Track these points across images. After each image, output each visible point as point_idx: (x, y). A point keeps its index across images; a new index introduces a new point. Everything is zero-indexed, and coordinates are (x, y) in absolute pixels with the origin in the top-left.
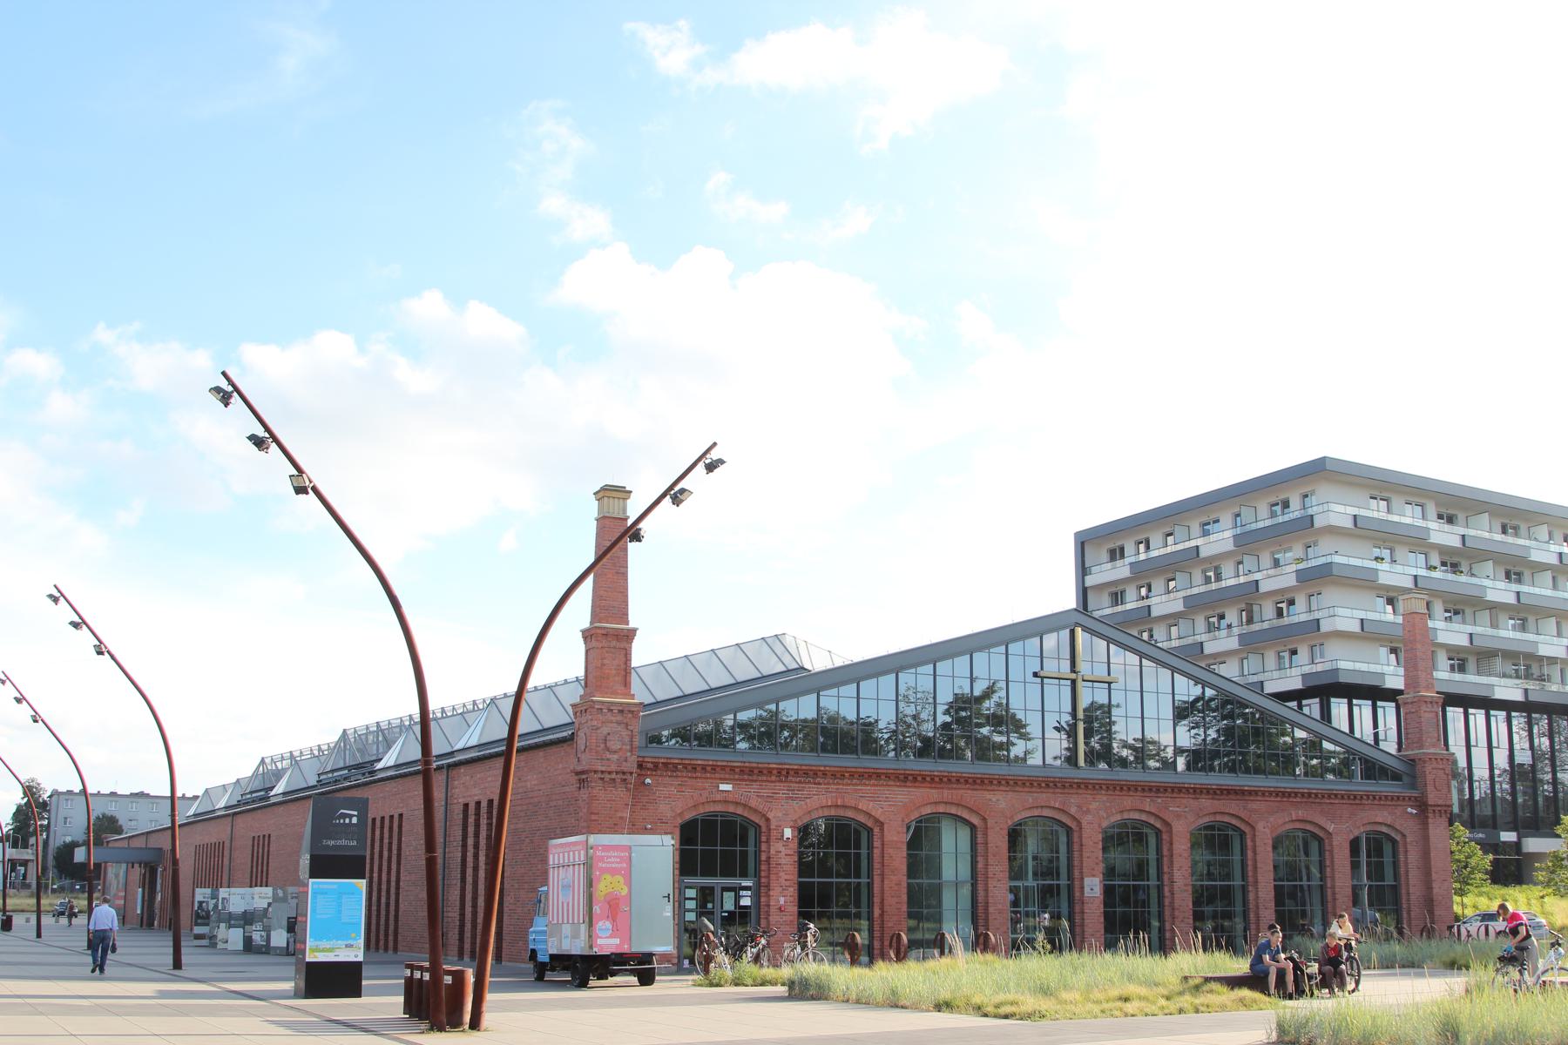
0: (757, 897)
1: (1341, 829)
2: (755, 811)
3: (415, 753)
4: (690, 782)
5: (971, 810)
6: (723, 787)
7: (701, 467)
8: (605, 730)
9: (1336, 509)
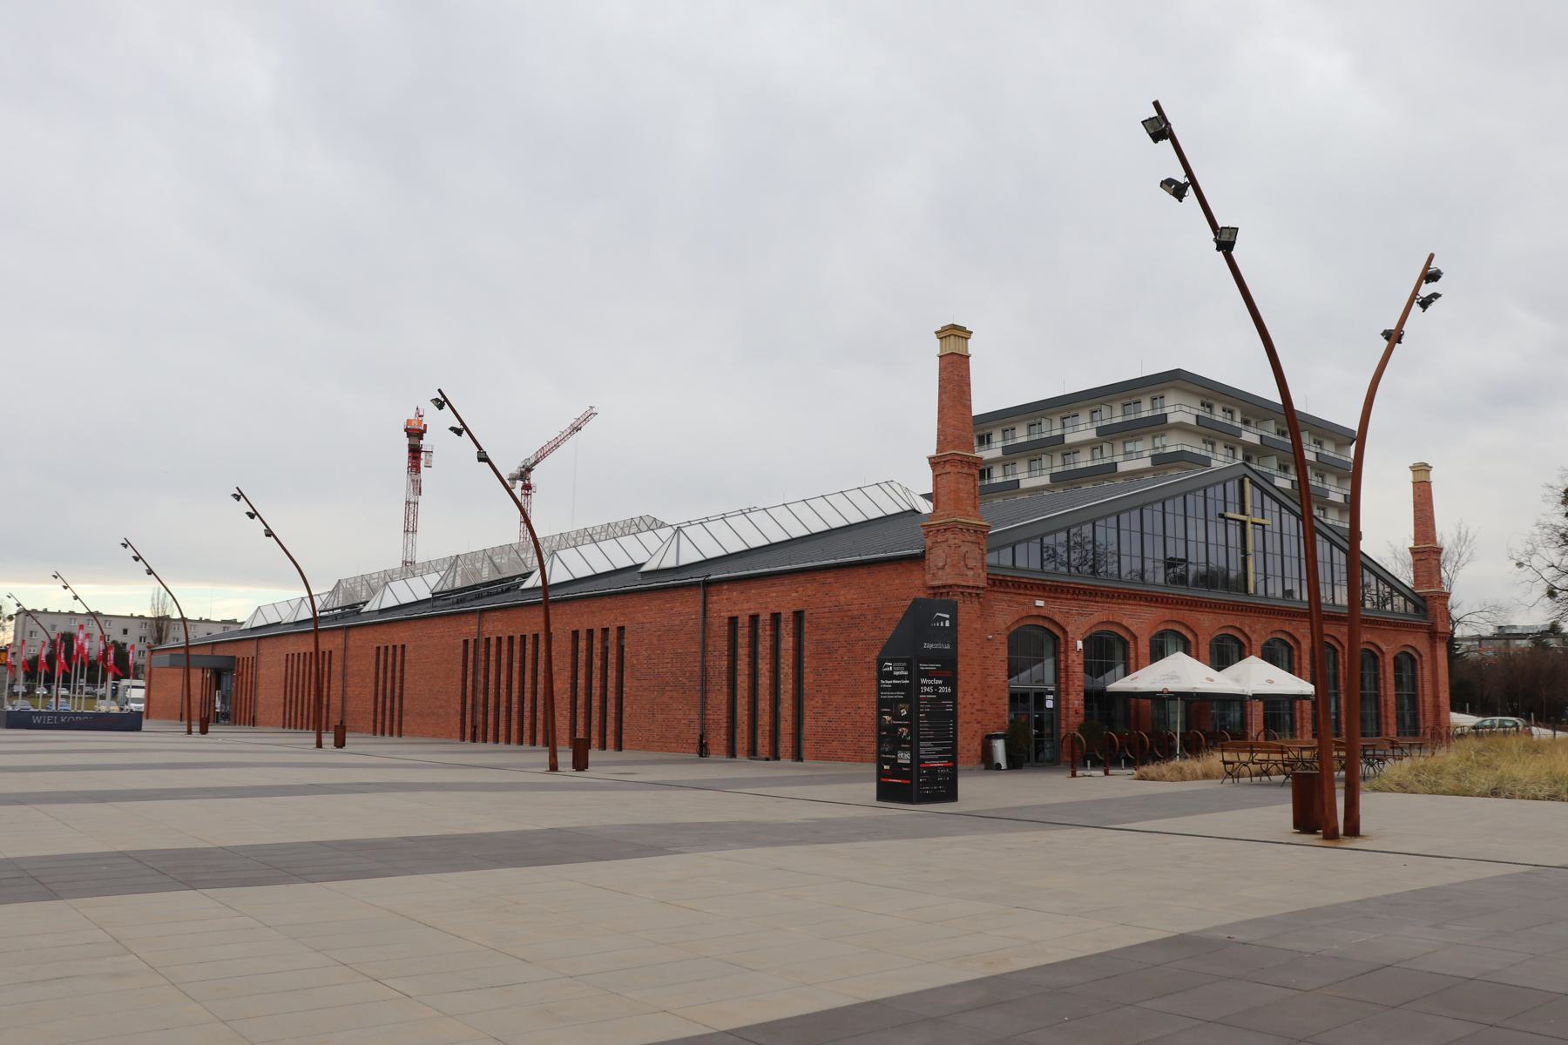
0: (1057, 701)
1: (1389, 648)
2: (1057, 624)
3: (540, 583)
4: (1017, 598)
5: (1188, 628)
6: (1040, 603)
7: (1416, 308)
8: (963, 549)
9: (1180, 410)
